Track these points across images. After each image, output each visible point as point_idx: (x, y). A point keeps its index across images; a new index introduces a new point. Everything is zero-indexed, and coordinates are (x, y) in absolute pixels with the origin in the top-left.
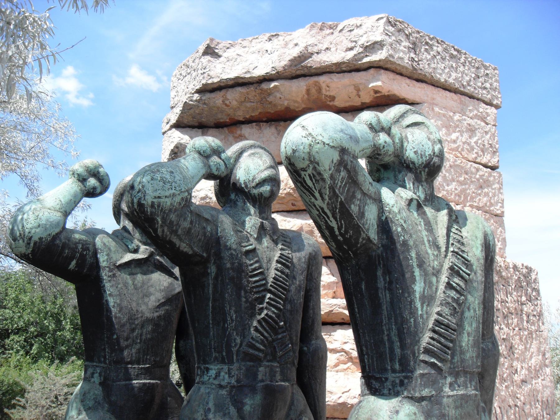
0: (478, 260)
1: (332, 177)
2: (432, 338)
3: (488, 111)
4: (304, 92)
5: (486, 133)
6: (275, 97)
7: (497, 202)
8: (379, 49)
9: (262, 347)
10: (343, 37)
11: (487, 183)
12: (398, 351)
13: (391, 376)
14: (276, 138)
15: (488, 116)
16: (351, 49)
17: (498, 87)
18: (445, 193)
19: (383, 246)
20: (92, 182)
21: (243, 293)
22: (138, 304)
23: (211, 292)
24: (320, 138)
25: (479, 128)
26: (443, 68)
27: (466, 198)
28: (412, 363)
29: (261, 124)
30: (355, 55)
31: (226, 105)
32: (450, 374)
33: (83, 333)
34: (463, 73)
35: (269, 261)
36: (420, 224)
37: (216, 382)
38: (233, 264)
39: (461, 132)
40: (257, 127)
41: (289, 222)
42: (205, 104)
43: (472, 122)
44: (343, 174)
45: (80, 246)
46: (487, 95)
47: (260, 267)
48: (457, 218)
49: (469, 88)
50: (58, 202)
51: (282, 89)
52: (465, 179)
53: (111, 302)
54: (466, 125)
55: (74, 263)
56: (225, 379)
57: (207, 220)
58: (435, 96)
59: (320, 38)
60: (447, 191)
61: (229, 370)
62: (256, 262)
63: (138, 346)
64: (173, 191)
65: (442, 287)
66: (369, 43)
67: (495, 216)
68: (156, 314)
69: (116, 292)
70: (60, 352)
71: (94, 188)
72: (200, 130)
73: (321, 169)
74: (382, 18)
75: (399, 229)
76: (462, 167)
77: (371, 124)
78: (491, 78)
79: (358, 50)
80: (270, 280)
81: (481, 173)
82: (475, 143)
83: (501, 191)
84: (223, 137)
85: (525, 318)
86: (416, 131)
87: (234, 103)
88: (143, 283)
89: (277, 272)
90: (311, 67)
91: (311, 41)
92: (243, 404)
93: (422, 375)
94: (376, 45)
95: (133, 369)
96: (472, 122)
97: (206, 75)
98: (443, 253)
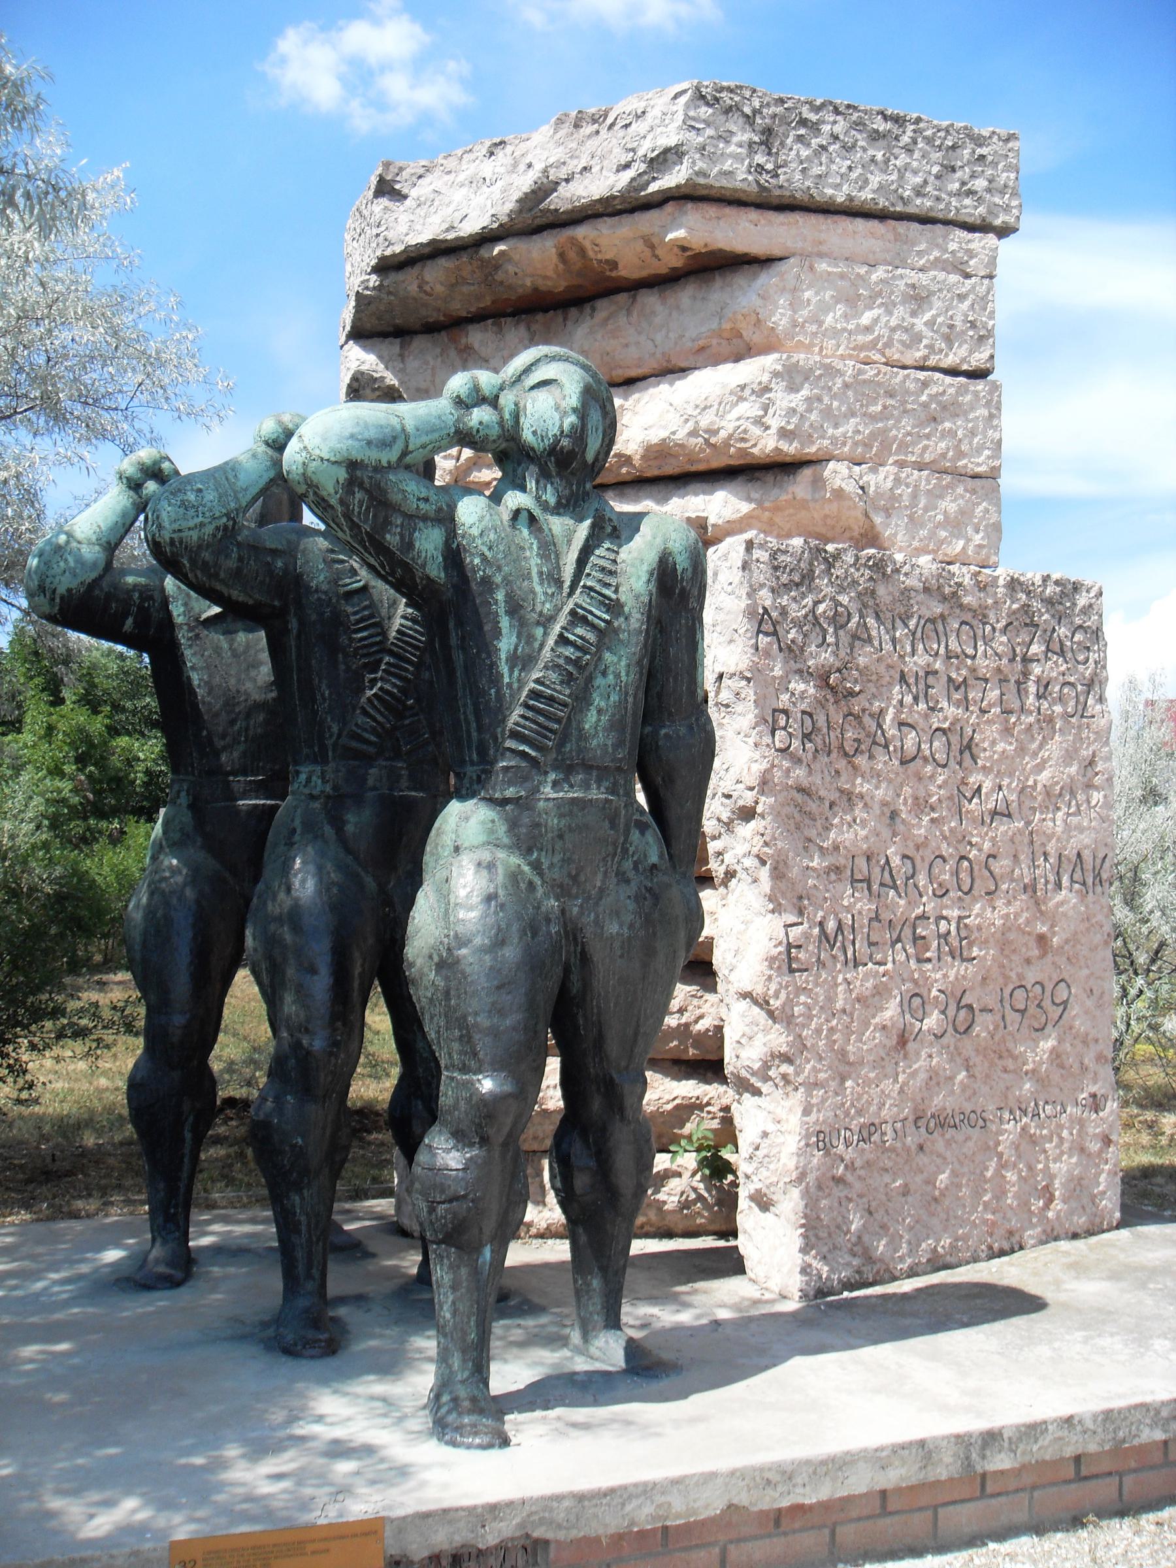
0: (637, 597)
1: (342, 502)
2: (523, 716)
3: (971, 246)
4: (555, 259)
5: (962, 297)
6: (506, 272)
8: (675, 164)
9: (373, 738)
10: (614, 141)
11: (952, 409)
12: (474, 734)
15: (971, 258)
16: (627, 166)
18: (826, 442)
19: (453, 586)
22: (239, 680)
24: (317, 452)
25: (940, 290)
27: (886, 447)
28: (492, 752)
30: (633, 179)
32: (555, 768)
34: (902, 172)
36: (531, 548)
37: (307, 791)
39: (889, 308)
42: (389, 293)
43: (924, 279)
44: (359, 495)
46: (976, 208)
47: (372, 616)
48: (615, 528)
49: (918, 201)
50: (95, 527)
51: (516, 257)
52: (885, 407)
53: (195, 678)
55: (130, 621)
57: (274, 552)
58: (823, 236)
59: (574, 145)
62: (365, 608)
63: (242, 747)
64: (201, 519)
65: (551, 642)
67: (973, 477)
69: (201, 664)
73: (324, 493)
74: (685, 91)
75: (477, 561)
76: (879, 384)
77: (458, 396)
78: (994, 164)
83: (995, 422)
84: (439, 350)
85: (1032, 689)
87: (440, 289)
88: (248, 646)
89: (403, 621)
90: (556, 210)
91: (556, 154)
92: (344, 823)
93: (506, 769)
95: (239, 782)
96: (924, 279)
97: (381, 238)
98: (566, 589)
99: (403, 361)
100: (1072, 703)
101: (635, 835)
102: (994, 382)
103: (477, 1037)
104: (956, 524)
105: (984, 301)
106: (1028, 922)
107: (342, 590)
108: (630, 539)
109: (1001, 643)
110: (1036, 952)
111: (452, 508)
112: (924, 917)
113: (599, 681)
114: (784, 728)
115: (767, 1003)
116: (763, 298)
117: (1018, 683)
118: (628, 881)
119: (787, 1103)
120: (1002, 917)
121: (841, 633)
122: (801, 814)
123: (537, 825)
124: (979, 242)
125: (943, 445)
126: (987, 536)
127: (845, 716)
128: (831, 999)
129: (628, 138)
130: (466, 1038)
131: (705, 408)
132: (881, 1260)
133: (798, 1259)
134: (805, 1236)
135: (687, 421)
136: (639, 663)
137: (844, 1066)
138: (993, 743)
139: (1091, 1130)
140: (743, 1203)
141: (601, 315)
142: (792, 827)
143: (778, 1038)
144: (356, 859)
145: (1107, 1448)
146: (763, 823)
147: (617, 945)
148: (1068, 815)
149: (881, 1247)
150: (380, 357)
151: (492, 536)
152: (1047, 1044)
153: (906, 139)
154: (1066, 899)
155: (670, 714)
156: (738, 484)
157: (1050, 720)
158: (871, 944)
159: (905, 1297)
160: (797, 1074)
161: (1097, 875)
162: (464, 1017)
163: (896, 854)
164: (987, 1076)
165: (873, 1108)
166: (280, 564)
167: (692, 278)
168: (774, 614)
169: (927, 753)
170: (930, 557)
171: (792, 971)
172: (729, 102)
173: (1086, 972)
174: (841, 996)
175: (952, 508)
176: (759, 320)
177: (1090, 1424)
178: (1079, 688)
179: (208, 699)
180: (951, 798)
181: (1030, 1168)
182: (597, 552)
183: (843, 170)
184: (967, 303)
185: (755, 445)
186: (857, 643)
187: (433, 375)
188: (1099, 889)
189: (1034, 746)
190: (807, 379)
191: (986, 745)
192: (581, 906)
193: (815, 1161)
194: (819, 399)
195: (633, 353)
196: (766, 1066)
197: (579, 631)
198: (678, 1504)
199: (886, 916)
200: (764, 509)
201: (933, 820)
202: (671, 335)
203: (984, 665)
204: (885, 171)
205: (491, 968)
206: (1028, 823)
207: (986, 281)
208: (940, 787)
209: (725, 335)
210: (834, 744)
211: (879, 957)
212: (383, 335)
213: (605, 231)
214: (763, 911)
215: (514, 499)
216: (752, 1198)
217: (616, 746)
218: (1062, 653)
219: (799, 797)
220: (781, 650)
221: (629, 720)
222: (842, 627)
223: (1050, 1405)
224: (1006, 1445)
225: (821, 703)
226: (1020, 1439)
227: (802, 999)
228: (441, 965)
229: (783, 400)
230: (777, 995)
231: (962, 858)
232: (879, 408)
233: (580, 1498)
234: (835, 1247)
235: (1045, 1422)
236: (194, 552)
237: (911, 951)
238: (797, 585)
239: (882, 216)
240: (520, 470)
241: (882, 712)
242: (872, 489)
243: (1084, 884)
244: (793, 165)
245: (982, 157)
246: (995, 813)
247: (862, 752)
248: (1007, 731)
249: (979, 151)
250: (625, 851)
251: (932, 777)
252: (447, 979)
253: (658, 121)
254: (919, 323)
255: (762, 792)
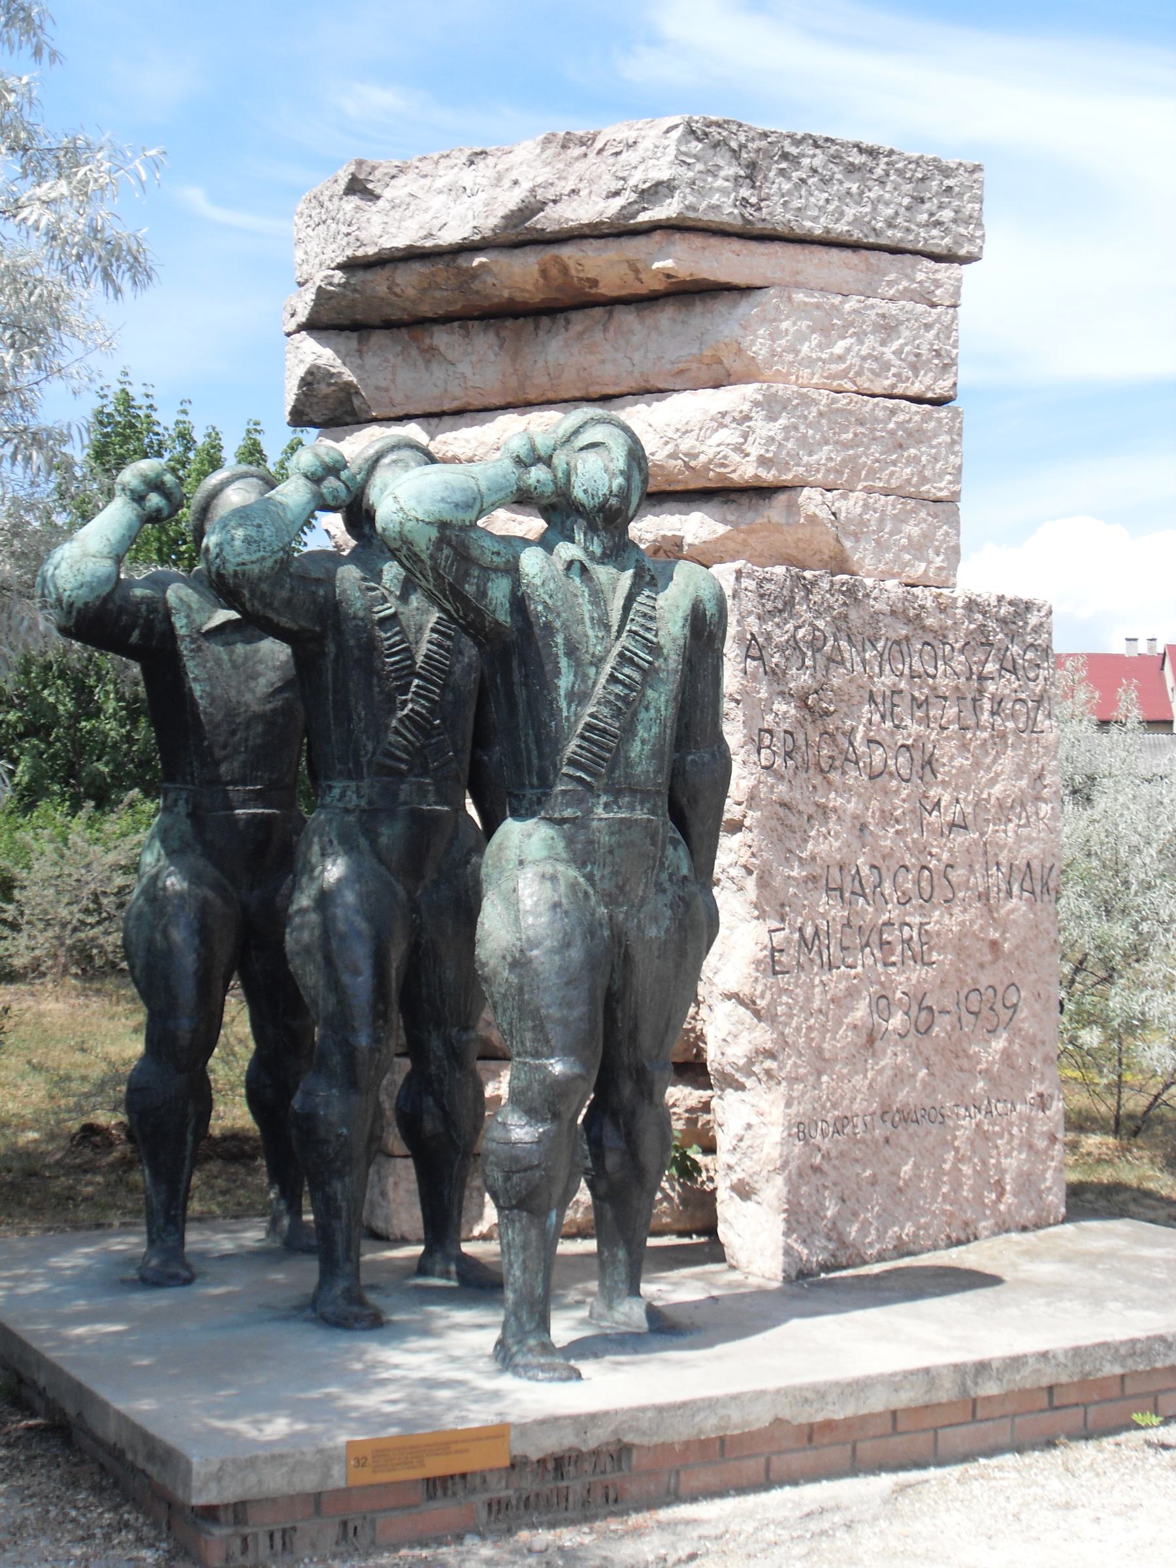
0: (674, 640)
1: (431, 557)
2: (579, 746)
3: (938, 276)
5: (928, 327)
6: (484, 282)
7: (944, 472)
8: (666, 197)
9: (405, 756)
10: (603, 167)
11: (917, 436)
12: (535, 761)
13: (529, 792)
14: (496, 355)
15: (938, 287)
16: (617, 194)
17: (975, 214)
18: (801, 469)
20: (154, 500)
21: (375, 680)
22: (239, 692)
23: (330, 680)
24: (413, 513)
25: (908, 320)
26: (821, 203)
27: (855, 472)
29: (470, 323)
30: (623, 208)
31: (396, 294)
33: (154, 722)
34: (875, 203)
35: (420, 629)
37: (341, 805)
38: (358, 640)
39: (860, 337)
40: (462, 332)
41: (520, 523)
42: (355, 290)
43: (892, 309)
45: (144, 608)
46: (943, 238)
47: (402, 642)
48: (653, 578)
49: (890, 233)
50: (105, 542)
51: (496, 269)
52: (856, 435)
53: (197, 689)
54: (874, 317)
55: (136, 633)
56: (353, 800)
59: (561, 166)
60: (807, 465)
61: (358, 788)
62: (395, 634)
63: (242, 757)
65: (602, 680)
66: (648, 185)
68: (269, 706)
70: (94, 780)
71: (159, 510)
72: (355, 335)
73: (417, 549)
74: (676, 126)
75: (540, 608)
76: (851, 412)
78: (960, 195)
79: (628, 197)
80: (420, 659)
81: (901, 417)
82: (894, 353)
83: (957, 448)
85: (987, 705)
86: (591, 457)
88: (246, 658)
91: (544, 174)
92: (378, 835)
93: (564, 792)
94: (660, 188)
96: (892, 309)
97: (352, 239)
98: (614, 634)
99: (361, 357)
100: (1023, 719)
101: (670, 851)
102: (956, 409)
103: (549, 1026)
104: (918, 548)
105: (948, 329)
106: (982, 928)
107: (376, 617)
108: (665, 587)
109: (960, 663)
110: (989, 958)
111: (517, 559)
112: (889, 923)
113: (643, 715)
114: (769, 747)
115: (754, 1003)
116: (744, 328)
117: (974, 700)
118: (664, 891)
119: (770, 1097)
120: (958, 924)
121: (818, 656)
122: (785, 824)
123: (591, 842)
124: (944, 271)
125: (908, 470)
126: (947, 558)
127: (821, 735)
128: (809, 999)
129: (618, 166)
130: (539, 1028)
131: (687, 432)
132: (854, 1246)
133: (780, 1240)
134: (787, 1221)
135: (667, 443)
136: (675, 698)
137: (821, 1062)
138: (952, 759)
139: (1038, 1128)
140: (723, 1195)
141: (576, 328)
142: (775, 839)
143: (763, 1036)
144: (389, 869)
145: (1076, 1379)
146: (751, 835)
147: (655, 947)
148: (1019, 826)
149: (853, 1231)
150: (337, 352)
151: (552, 586)
152: (999, 1044)
153: (879, 172)
154: (1016, 906)
155: (696, 742)
156: (714, 506)
157: (1003, 736)
158: (843, 949)
159: (877, 1277)
160: (780, 1069)
161: (1045, 884)
162: (538, 1010)
163: (864, 864)
164: (945, 1075)
165: (846, 1102)
166: (322, 592)
167: (671, 300)
168: (761, 640)
169: (893, 768)
170: (896, 581)
171: (775, 973)
172: (717, 137)
173: (1034, 976)
174: (818, 997)
175: (916, 532)
176: (740, 350)
177: (1062, 1359)
178: (1030, 704)
179: (210, 710)
180: (913, 811)
181: (984, 1163)
182: (639, 599)
183: (821, 203)
184: (933, 332)
185: (734, 471)
186: (832, 665)
187: (394, 374)
188: (1046, 897)
189: (988, 760)
190: (785, 408)
191: (945, 760)
192: (626, 913)
193: (796, 1150)
194: (796, 428)
195: (609, 371)
196: (751, 1062)
197: (627, 671)
198: (736, 1416)
199: (856, 922)
200: (740, 531)
201: (897, 832)
202: (650, 355)
203: (944, 684)
204: (859, 203)
205: (561, 967)
206: (982, 834)
207: (951, 311)
208: (904, 801)
209: (706, 361)
210: (812, 761)
211: (850, 960)
212: (339, 328)
213: (590, 253)
214: (748, 917)
215: (567, 551)
216: (733, 1188)
217: (656, 772)
218: (1014, 671)
219: (782, 812)
220: (766, 673)
221: (667, 749)
222: (819, 650)
223: (1027, 1343)
224: (994, 1373)
225: (800, 723)
226: (1005, 1370)
227: (785, 999)
228: (515, 965)
229: (763, 428)
230: (762, 996)
231: (924, 867)
232: (851, 436)
233: (660, 1409)
234: (813, 1232)
235: (1026, 1356)
236: (253, 583)
237: (878, 954)
238: (780, 611)
239: (855, 246)
240: (568, 523)
241: (853, 730)
242: (843, 515)
243: (1033, 893)
244: (775, 198)
245: (949, 189)
246: (952, 825)
247: (836, 769)
248: (964, 747)
249: (947, 182)
250: (662, 864)
251: (897, 792)
252: (520, 976)
253: (649, 154)
254: (888, 352)
255: (750, 807)
